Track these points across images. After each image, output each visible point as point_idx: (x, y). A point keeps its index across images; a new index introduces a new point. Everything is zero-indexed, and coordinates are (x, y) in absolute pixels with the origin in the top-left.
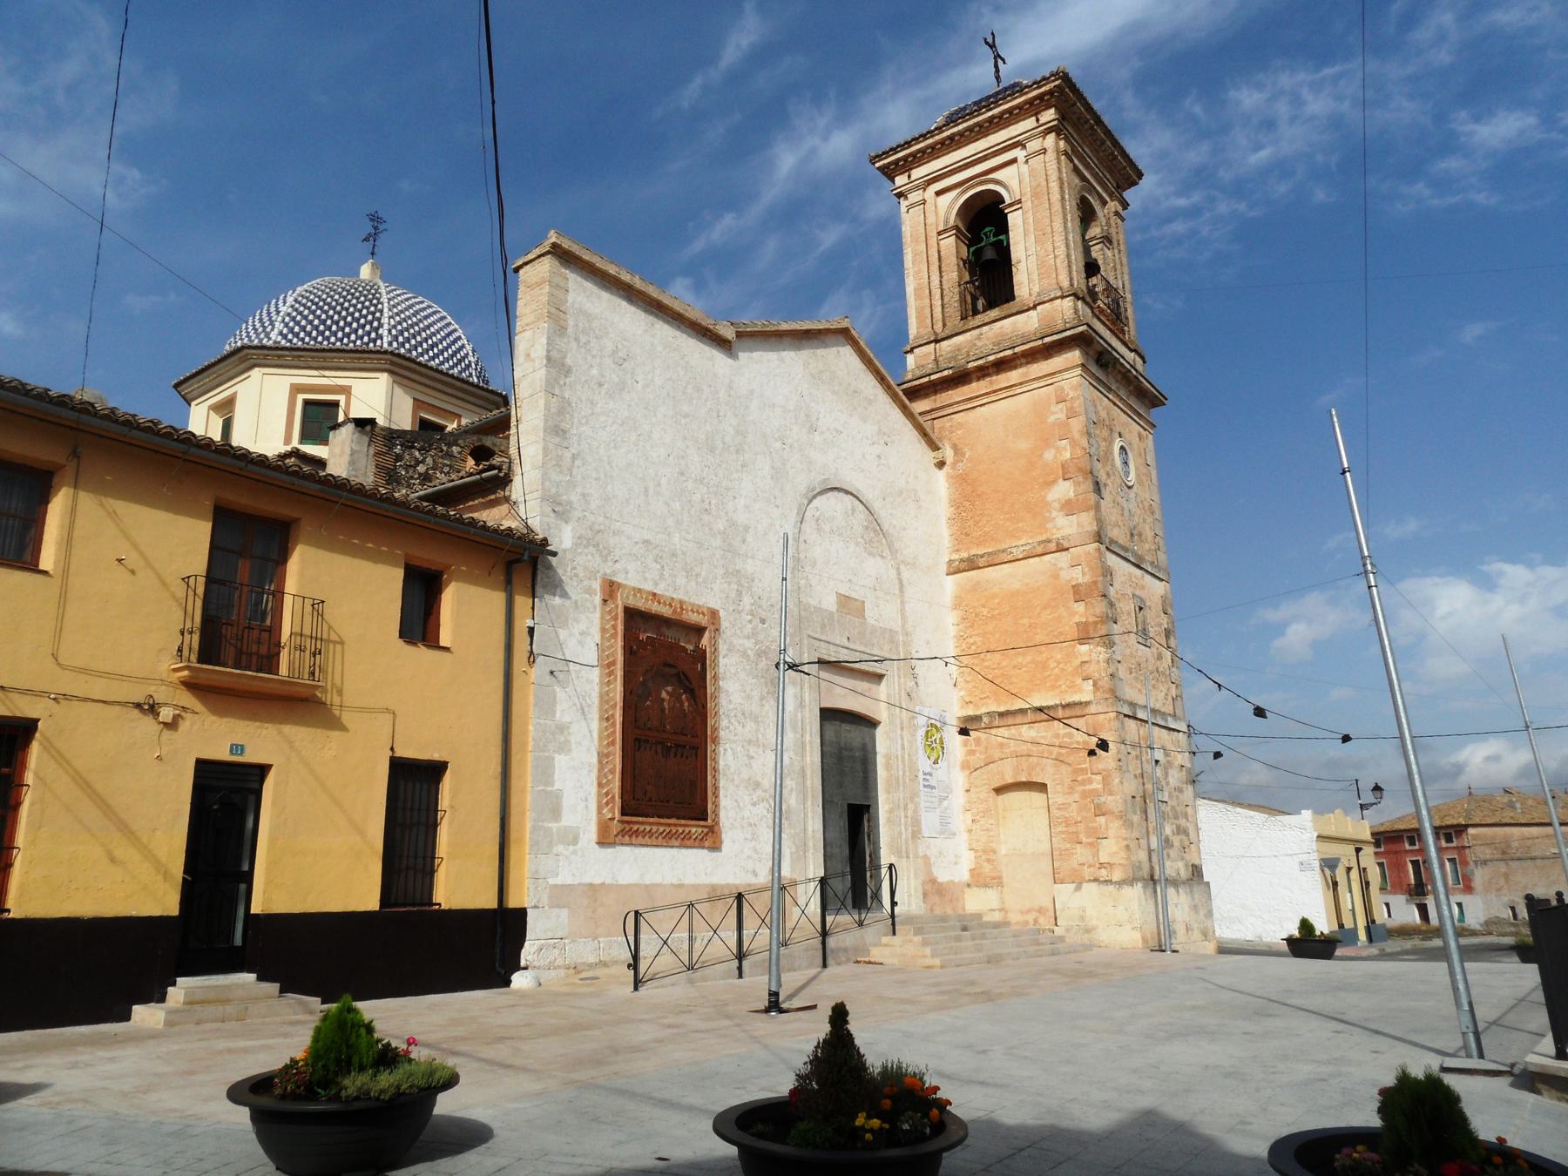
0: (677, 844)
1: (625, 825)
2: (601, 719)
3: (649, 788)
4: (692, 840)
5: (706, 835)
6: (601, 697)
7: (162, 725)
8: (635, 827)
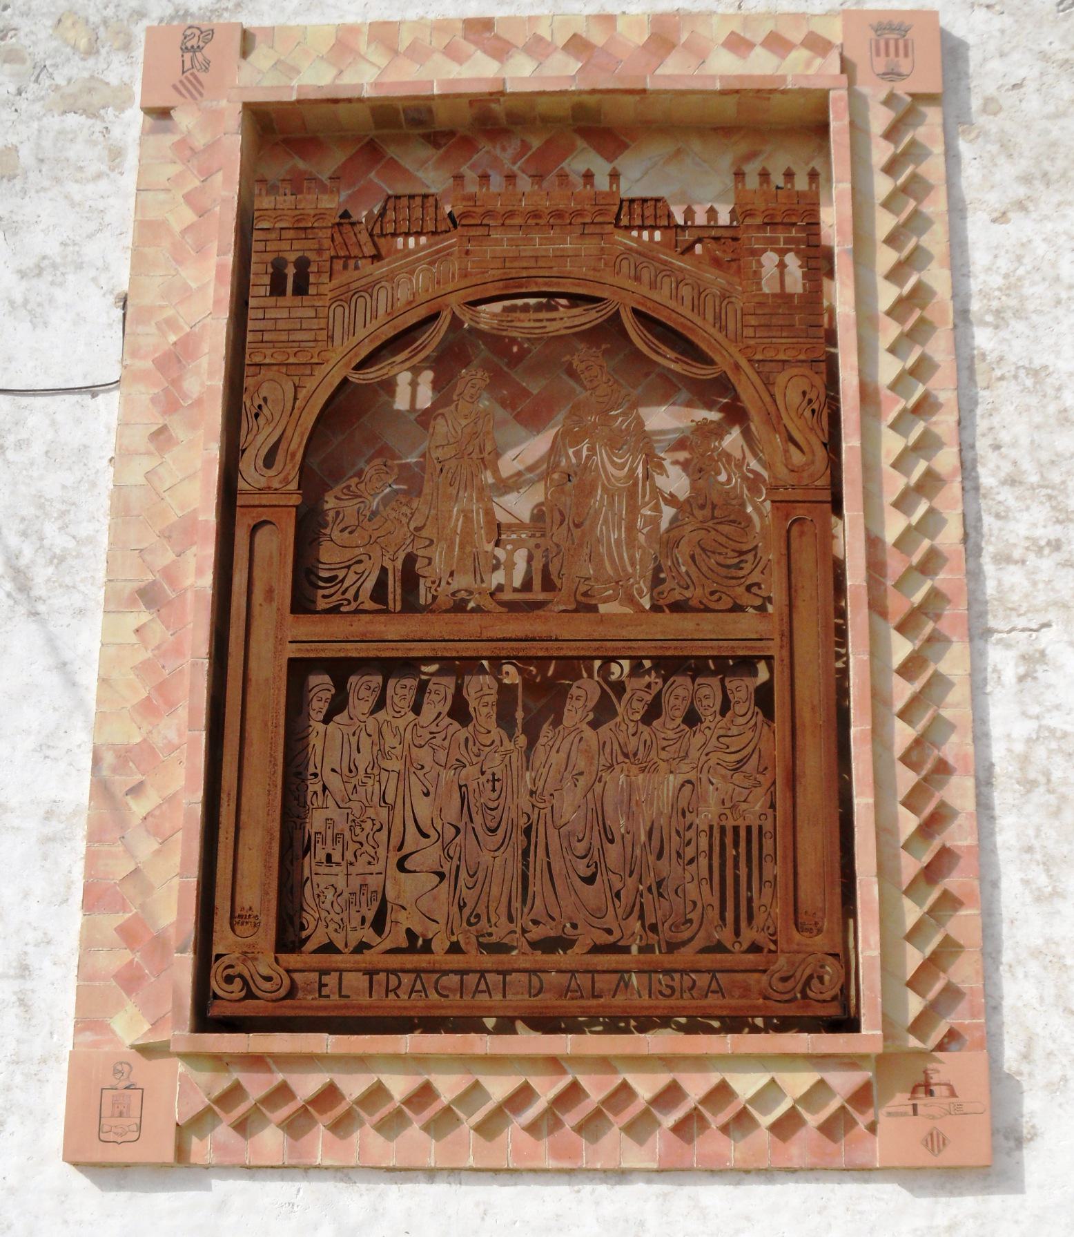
0: (635, 1156)
1: (238, 1075)
2: (115, 604)
3: (403, 888)
4: (762, 1136)
5: (862, 1097)
6: (122, 510)
7: (1055, 871)
8: (308, 1085)
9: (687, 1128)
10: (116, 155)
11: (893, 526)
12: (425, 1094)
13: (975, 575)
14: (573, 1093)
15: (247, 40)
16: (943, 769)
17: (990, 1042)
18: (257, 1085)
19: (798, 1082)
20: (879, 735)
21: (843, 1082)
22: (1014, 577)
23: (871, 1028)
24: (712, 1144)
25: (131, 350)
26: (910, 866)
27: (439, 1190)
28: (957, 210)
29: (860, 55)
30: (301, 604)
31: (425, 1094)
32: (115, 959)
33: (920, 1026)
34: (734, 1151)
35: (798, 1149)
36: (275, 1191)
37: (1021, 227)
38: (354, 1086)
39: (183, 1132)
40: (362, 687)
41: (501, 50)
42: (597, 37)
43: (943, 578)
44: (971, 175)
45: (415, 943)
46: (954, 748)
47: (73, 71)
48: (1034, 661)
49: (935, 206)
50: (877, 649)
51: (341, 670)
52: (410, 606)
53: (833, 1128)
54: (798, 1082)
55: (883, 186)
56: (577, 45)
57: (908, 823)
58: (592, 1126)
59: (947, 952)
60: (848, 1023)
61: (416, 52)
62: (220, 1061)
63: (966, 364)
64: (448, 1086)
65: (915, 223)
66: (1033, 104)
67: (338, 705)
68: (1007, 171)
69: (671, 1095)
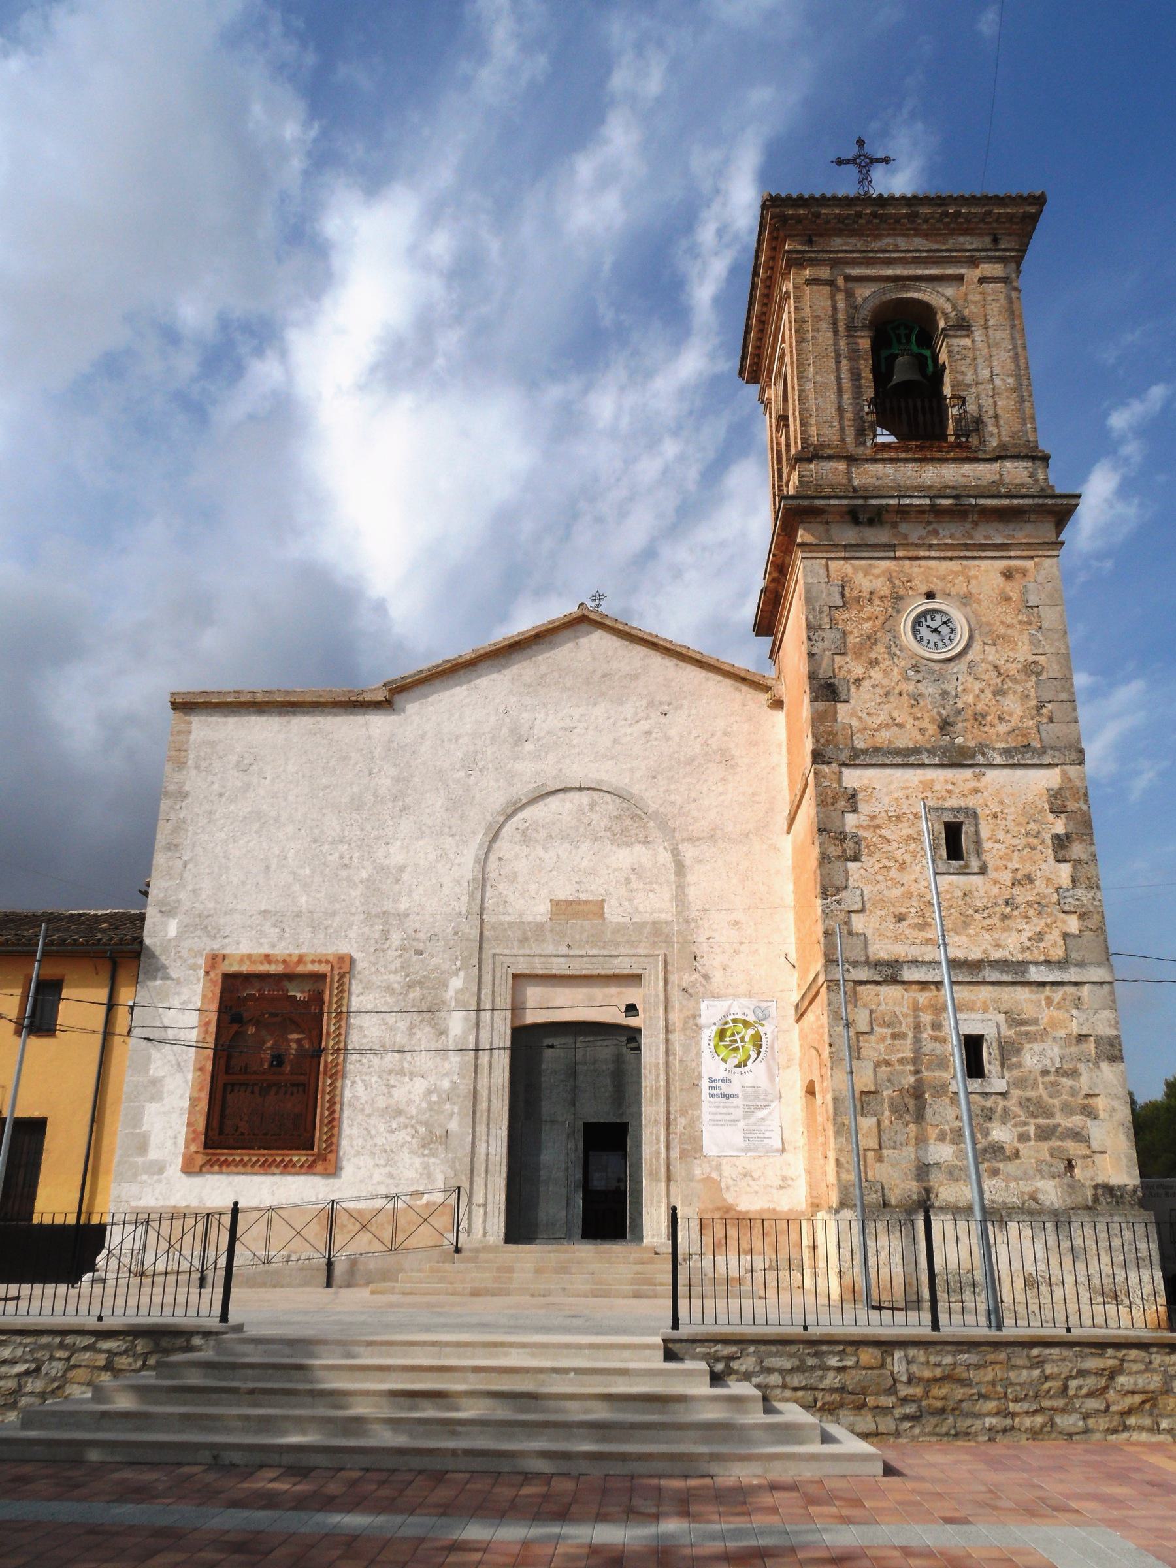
2: (195, 1070)
5: (314, 1161)
8: (223, 1158)
9: (286, 1166)
10: (199, 980)
11: (330, 1058)
12: (242, 1160)
13: (344, 1067)
14: (266, 1160)
15: (224, 957)
16: (335, 1103)
17: (337, 1152)
18: (214, 1159)
19: (304, 1159)
20: (323, 1097)
21: (311, 1159)
22: (352, 1067)
23: (316, 1150)
24: (289, 1169)
25: (200, 1021)
26: (326, 1121)
27: (243, 1177)
28: (350, 994)
29: (335, 963)
30: (227, 1072)
31: (242, 1160)
32: (192, 1136)
33: (325, 1149)
34: (293, 1170)
35: (303, 1170)
36: (216, 1177)
37: (362, 998)
38: (230, 1159)
39: (202, 1166)
40: (236, 1088)
41: (270, 962)
42: (288, 959)
43: (339, 1068)
44: (354, 987)
45: (243, 1134)
46: (337, 1099)
47: (191, 961)
48: (353, 1083)
49: (346, 995)
50: (324, 1082)
51: (233, 1085)
52: (246, 1073)
53: (310, 1167)
54: (304, 1159)
55: (336, 992)
56: (284, 962)
57: (327, 1113)
58: (270, 1165)
59: (332, 1135)
60: (312, 1148)
61: (254, 962)
62: (207, 1154)
63: (348, 1025)
64: (246, 1159)
65: (341, 999)
66: (367, 972)
67: (232, 1091)
68: (360, 987)
69: (282, 1161)
